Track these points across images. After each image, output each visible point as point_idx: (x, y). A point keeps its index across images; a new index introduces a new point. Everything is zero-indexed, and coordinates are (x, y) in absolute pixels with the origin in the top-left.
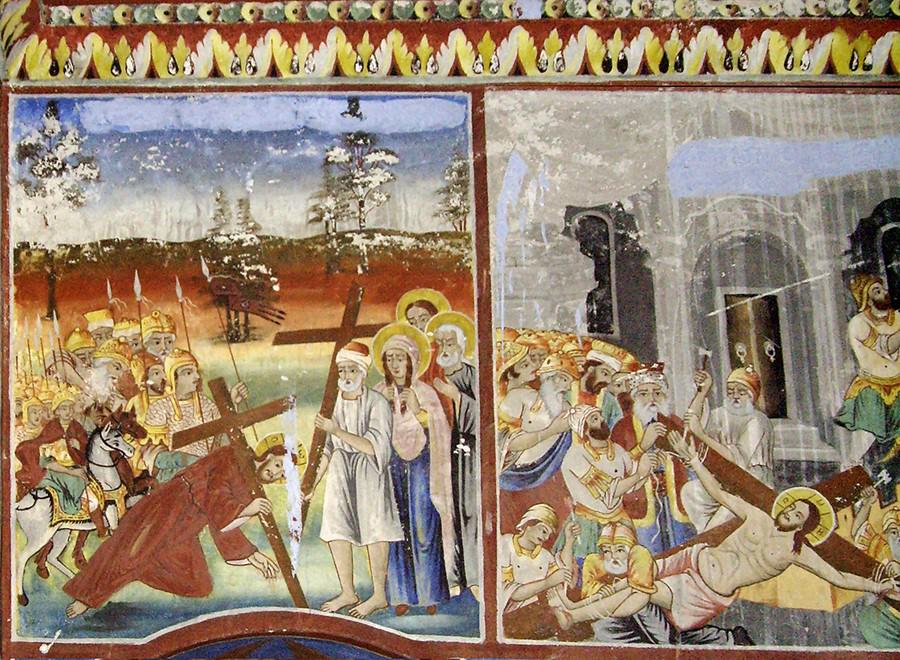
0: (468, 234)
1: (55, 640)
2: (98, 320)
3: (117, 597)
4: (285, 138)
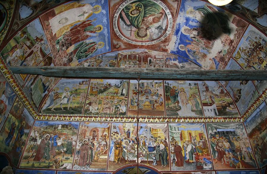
0: (244, 64)
1: (262, 167)
2: (254, 137)
3: (263, 161)
4: (257, 114)
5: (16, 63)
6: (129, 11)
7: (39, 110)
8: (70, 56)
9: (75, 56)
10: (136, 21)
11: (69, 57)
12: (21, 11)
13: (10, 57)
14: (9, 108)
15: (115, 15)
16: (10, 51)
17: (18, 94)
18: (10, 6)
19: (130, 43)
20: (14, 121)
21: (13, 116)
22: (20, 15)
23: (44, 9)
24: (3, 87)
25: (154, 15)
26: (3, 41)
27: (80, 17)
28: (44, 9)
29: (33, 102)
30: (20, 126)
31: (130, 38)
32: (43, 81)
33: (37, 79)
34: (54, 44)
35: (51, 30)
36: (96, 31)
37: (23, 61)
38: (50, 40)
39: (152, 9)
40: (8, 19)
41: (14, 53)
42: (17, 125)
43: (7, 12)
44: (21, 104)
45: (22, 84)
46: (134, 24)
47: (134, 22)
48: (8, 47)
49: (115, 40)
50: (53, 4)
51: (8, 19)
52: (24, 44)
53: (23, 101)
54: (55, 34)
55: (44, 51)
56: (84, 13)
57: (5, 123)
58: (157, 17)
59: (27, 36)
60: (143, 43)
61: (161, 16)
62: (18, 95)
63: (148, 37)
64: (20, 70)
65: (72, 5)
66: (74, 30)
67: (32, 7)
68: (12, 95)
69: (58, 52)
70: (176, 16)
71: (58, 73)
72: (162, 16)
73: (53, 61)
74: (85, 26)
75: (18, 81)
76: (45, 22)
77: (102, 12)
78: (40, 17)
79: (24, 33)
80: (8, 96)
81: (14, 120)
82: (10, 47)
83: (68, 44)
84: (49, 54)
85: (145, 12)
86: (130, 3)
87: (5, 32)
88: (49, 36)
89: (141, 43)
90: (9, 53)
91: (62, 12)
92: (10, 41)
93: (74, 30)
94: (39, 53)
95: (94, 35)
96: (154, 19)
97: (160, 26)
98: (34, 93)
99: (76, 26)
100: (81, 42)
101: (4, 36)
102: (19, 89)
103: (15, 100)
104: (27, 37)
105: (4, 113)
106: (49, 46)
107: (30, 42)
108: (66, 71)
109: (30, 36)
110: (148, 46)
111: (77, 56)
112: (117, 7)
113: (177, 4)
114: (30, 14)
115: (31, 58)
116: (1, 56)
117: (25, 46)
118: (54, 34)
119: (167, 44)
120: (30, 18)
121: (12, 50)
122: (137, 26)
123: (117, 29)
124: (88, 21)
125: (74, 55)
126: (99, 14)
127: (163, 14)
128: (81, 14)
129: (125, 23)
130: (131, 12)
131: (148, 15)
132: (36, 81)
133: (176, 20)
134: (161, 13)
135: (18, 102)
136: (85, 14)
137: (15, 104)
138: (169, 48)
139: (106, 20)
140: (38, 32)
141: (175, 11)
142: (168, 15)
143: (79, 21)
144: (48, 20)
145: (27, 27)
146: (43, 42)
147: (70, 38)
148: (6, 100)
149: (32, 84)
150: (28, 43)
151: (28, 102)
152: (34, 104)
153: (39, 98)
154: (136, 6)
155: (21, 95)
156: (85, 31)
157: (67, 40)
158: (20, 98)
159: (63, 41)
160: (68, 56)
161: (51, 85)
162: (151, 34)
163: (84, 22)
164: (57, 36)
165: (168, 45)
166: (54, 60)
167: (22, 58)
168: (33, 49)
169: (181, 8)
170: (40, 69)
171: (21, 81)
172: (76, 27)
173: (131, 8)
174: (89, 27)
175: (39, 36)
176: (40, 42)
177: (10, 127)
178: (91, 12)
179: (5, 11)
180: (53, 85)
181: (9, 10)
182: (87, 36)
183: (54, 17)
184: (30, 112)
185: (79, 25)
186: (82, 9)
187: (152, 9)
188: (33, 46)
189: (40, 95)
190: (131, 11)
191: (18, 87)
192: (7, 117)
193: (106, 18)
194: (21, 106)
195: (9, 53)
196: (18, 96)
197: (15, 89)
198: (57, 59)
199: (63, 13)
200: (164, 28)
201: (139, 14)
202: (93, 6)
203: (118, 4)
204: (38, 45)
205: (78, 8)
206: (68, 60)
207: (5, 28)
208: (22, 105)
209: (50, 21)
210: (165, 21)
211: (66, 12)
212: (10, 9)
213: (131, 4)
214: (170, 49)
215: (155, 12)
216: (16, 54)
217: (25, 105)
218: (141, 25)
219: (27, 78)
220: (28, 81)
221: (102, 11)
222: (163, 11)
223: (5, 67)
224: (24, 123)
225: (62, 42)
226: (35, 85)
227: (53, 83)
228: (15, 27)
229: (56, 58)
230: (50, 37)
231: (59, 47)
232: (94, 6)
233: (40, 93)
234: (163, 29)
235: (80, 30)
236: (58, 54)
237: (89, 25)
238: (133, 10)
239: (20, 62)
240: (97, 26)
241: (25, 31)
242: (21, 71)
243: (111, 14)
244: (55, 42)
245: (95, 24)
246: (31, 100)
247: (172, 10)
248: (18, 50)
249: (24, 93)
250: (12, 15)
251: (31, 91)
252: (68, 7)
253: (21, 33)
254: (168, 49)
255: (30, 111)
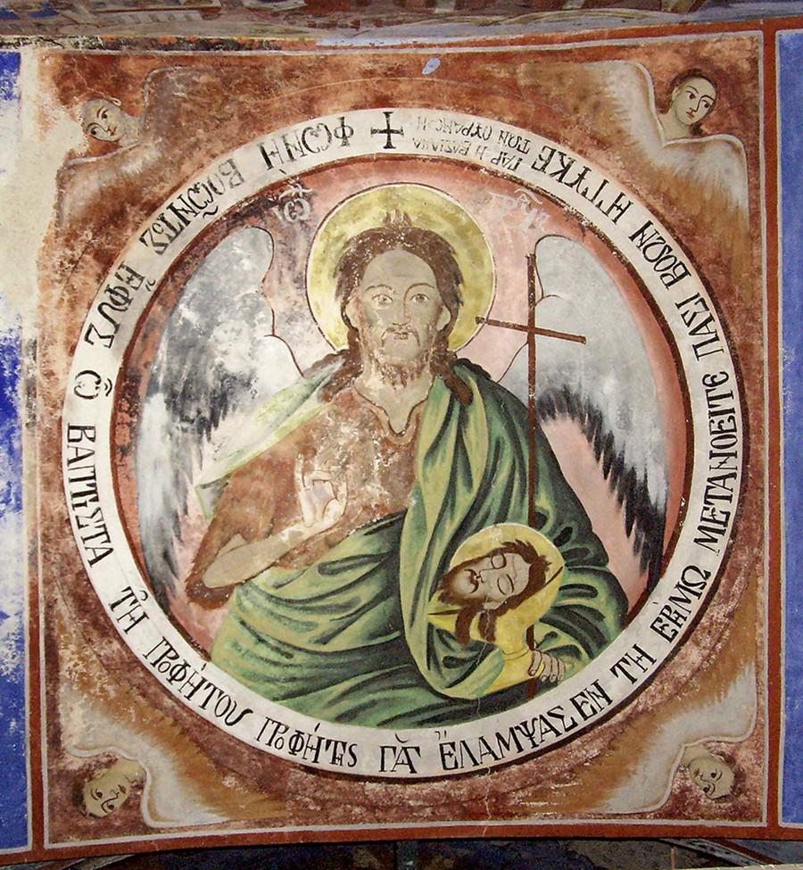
6: (565, 589)
10: (478, 463)
15: (711, 561)
19: (538, 144)
25: (285, 559)
31: (543, 221)
39: (310, 626)
46: (500, 429)
47: (497, 449)
49: (720, 205)
58: (248, 539)
60: (377, 146)
61: (204, 556)
63: (318, 246)
70: (50, 606)
72: (197, 560)
85: (391, 589)
86: (550, 684)
89: (402, 146)
96: (284, 506)
97: (206, 425)
110: (309, 108)
112: (693, 655)
113: (70, 741)
119: (88, 187)
122: (461, 397)
123: (695, 369)
127: (190, 591)
129: (603, 445)
130: (536, 582)
131: (356, 545)
133: (33, 555)
134: (216, 599)
138: (44, 122)
141: (67, 654)
142: (139, 586)
154: (491, 648)
162: (293, 292)
165: (63, 180)
169: (19, 719)
173: (541, 631)
187: (310, 626)
190: (546, 598)
200: (155, 411)
201: (454, 563)
203: (681, 687)
210: (151, 504)
213: (541, 672)
214: (29, 108)
215: (287, 592)
218: (415, 417)
222: (195, 625)
234: (159, 399)
238: (514, 602)
243: (764, 581)
247: (107, 666)
254: (61, 112)
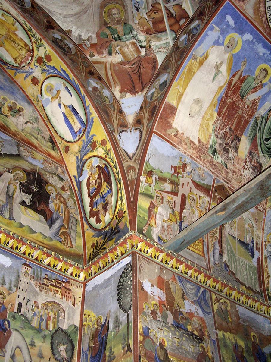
5: (170, 232)
7: (265, 295)
8: (251, 161)
9: (261, 154)
11: (253, 164)
12: (123, 145)
13: (154, 229)
14: (209, 320)
16: (149, 217)
17: (210, 286)
18: (105, 148)
20: (234, 341)
21: (226, 332)
22: (126, 152)
23: (152, 113)
24: (177, 287)
26: (128, 210)
27: (216, 79)
28: (152, 113)
29: (245, 285)
30: (250, 345)
32: (236, 236)
33: (223, 239)
34: (209, 158)
35: (187, 137)
36: (261, 82)
37: (179, 222)
38: (197, 157)
40: (115, 170)
41: (157, 218)
42: (243, 346)
43: (107, 161)
44: (225, 302)
45: (204, 264)
48: (141, 214)
50: (159, 95)
51: (115, 170)
52: (162, 193)
53: (226, 295)
54: (199, 141)
55: (202, 182)
56: (217, 67)
57: (219, 353)
59: (157, 177)
62: (209, 288)
64: (184, 241)
65: (187, 71)
66: (225, 108)
67: (135, 126)
68: (200, 293)
69: (225, 168)
71: (251, 199)
73: (228, 189)
74: (237, 88)
75: (195, 263)
76: (169, 131)
77: (246, 40)
78: (154, 130)
79: (150, 174)
80: (195, 299)
81: (231, 338)
82: (145, 212)
83: (232, 141)
84: (214, 182)
87: (122, 195)
88: (191, 150)
90: (149, 222)
91: (182, 95)
92: (139, 202)
93: (225, 108)
94: (195, 191)
95: (265, 90)
98: (236, 269)
99: (222, 99)
100: (252, 122)
101: (125, 201)
102: (205, 276)
103: (210, 299)
104: (159, 178)
105: (206, 333)
106: (205, 168)
107: (169, 183)
108: (262, 185)
109: (162, 172)
111: (264, 151)
112: (262, 9)
114: (139, 139)
115: (189, 210)
116: (141, 235)
117: (165, 195)
118: (196, 142)
120: (142, 145)
121: (151, 216)
124: (234, 76)
125: (258, 153)
126: (242, 48)
128: (214, 74)
132: (224, 245)
135: (218, 300)
136: (220, 69)
137: (216, 307)
139: (264, 47)
140: (169, 157)
143: (221, 88)
144: (170, 126)
145: (147, 162)
146: (188, 169)
147: (228, 127)
148: (196, 308)
149: (221, 254)
150: (168, 187)
151: (235, 290)
152: (249, 288)
153: (251, 273)
155: (215, 284)
156: (243, 97)
157: (225, 136)
158: (217, 292)
159: (220, 142)
160: (248, 164)
161: (257, 236)
163: (230, 83)
164: (204, 141)
166: (229, 187)
167: (174, 218)
168: (181, 192)
170: (214, 215)
171: (198, 259)
172: (222, 102)
174: (243, 85)
175: (177, 163)
176: (184, 171)
177: (233, 356)
178: (227, 56)
179: (104, 162)
180: (258, 233)
181: (108, 156)
182: (253, 103)
183: (175, 114)
184: (251, 308)
185: (226, 95)
186: (209, 65)
188: (178, 185)
189: (249, 266)
191: (200, 273)
192: (217, 339)
193: (260, 45)
194: (227, 306)
195: (149, 222)
196: (211, 289)
197: (198, 280)
198: (233, 181)
199: (184, 96)
202: (222, 44)
204: (184, 179)
205: (201, 68)
206: (254, 169)
207: (119, 186)
208: (228, 302)
209: (174, 125)
211: (188, 90)
212: (108, 154)
216: (160, 217)
217: (234, 299)
219: (206, 249)
220: (211, 253)
221: (244, 39)
223: (157, 251)
224: (254, 336)
225: (221, 145)
226: (228, 252)
227: (257, 230)
228: (131, 176)
229: (230, 181)
230: (194, 152)
231: (221, 157)
232: (223, 40)
233: (247, 262)
235: (234, 102)
236: (228, 170)
237: (242, 80)
239: (177, 227)
240: (257, 72)
241: (149, 170)
242: (186, 242)
243: (262, 31)
244: (209, 155)
245: (251, 71)
246: (240, 285)
248: (159, 208)
249: (218, 278)
250: (115, 160)
251: (229, 268)
252: (185, 80)
253: (145, 178)
255: (250, 306)
